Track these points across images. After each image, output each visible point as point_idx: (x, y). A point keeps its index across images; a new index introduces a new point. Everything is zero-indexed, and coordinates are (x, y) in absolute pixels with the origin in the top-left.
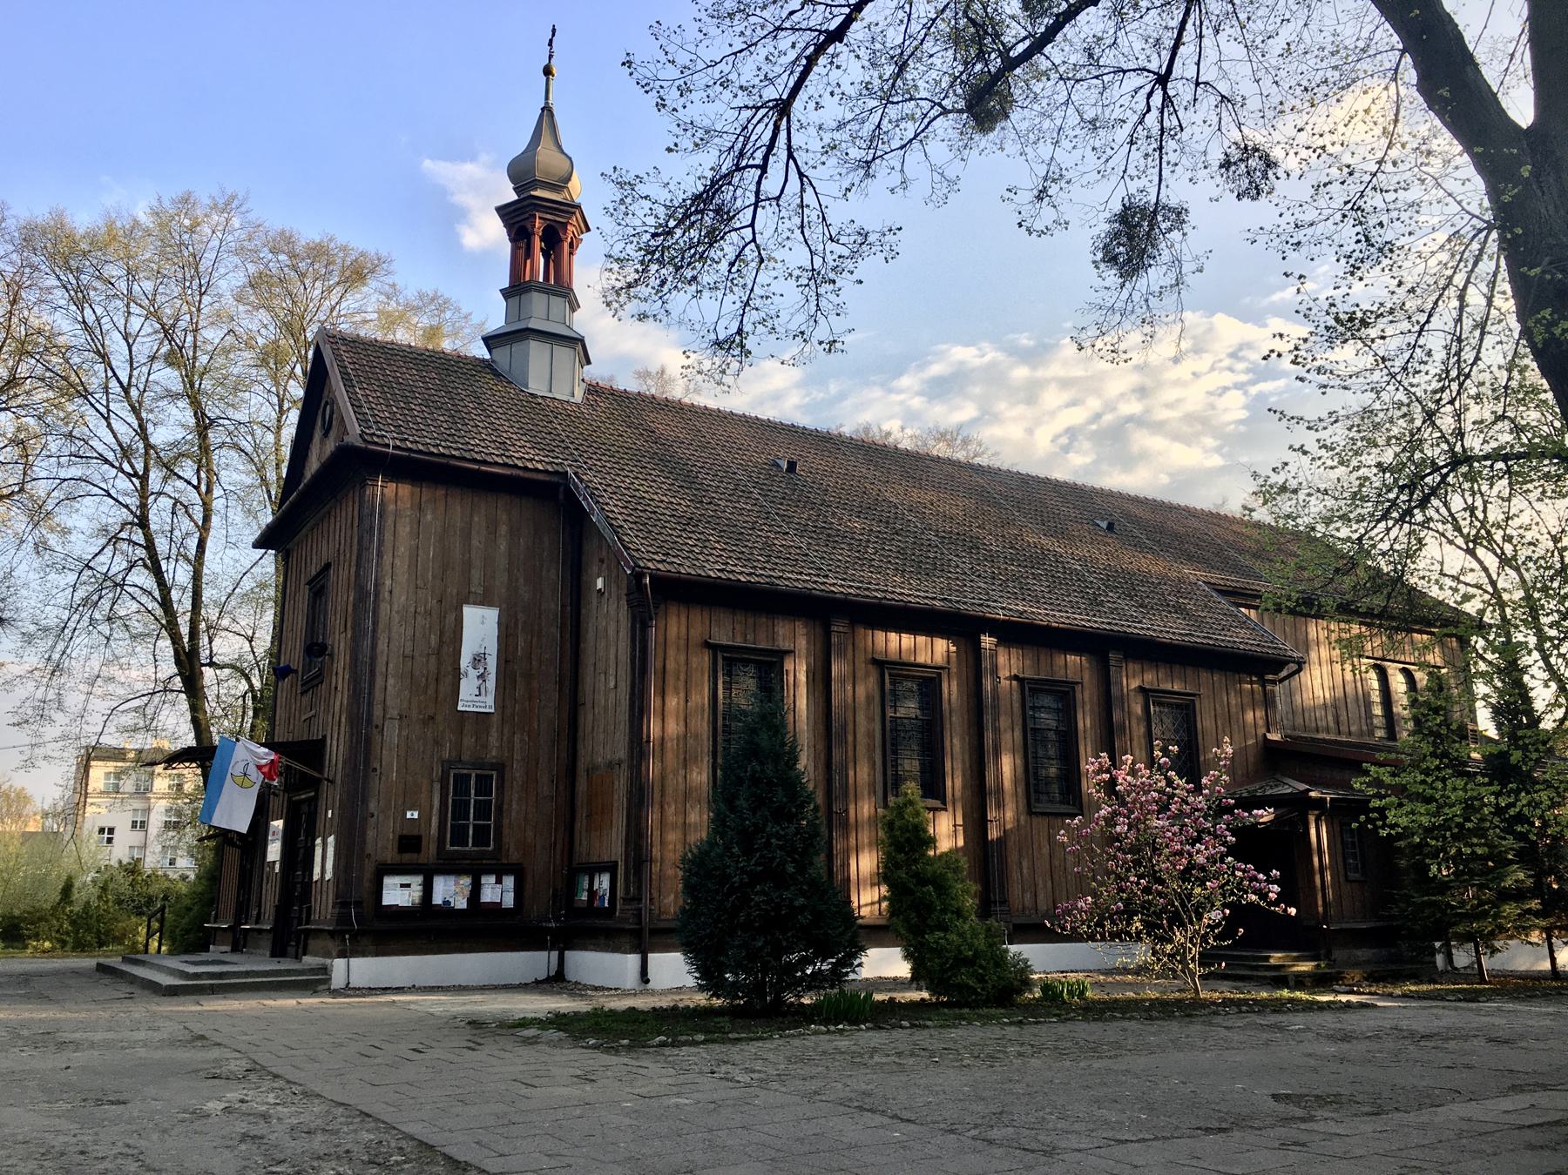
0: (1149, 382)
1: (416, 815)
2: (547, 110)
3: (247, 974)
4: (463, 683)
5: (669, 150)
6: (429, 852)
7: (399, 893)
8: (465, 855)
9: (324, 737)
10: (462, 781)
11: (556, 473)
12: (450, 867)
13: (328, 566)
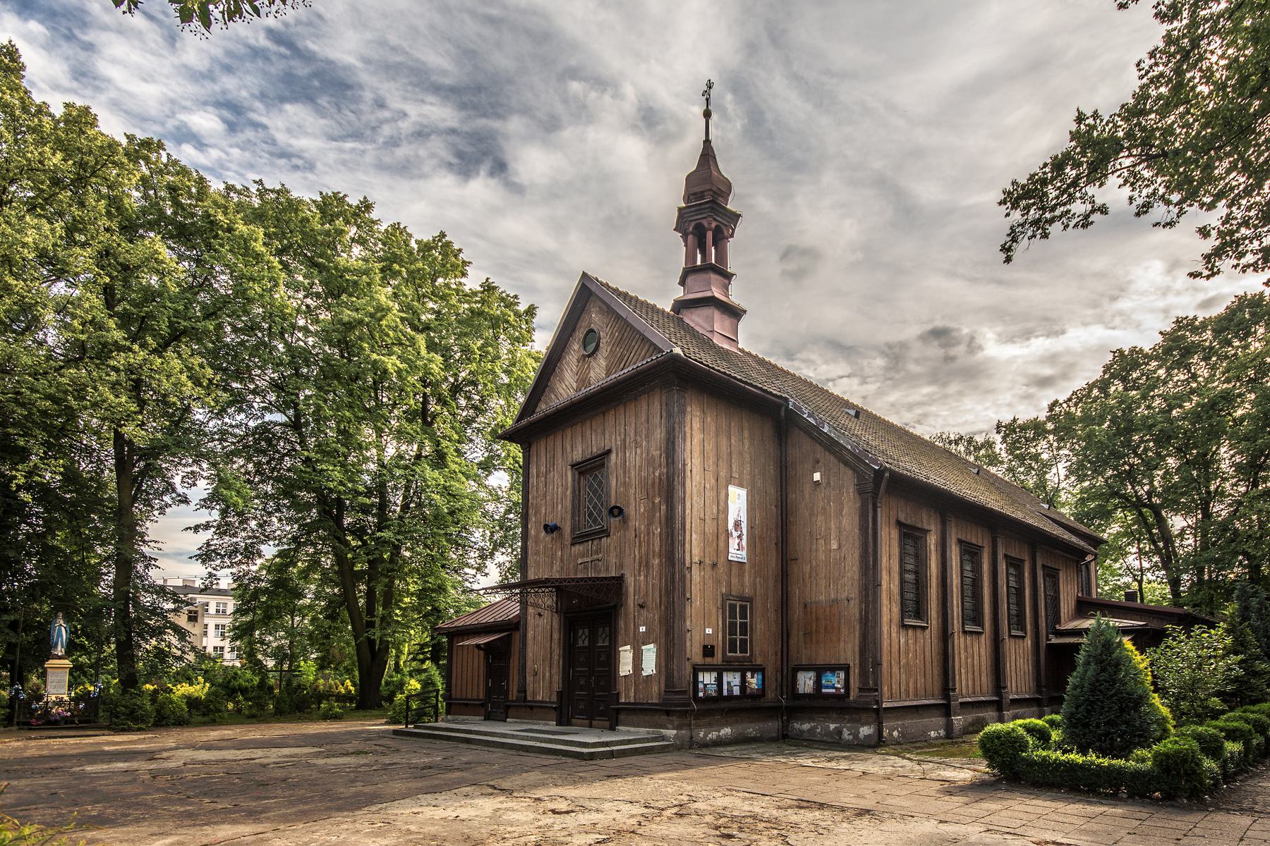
0: (217, 68)
2: (707, 142)
4: (731, 540)
5: (1008, 260)
8: (737, 659)
9: (623, 575)
10: (733, 607)
12: (728, 666)
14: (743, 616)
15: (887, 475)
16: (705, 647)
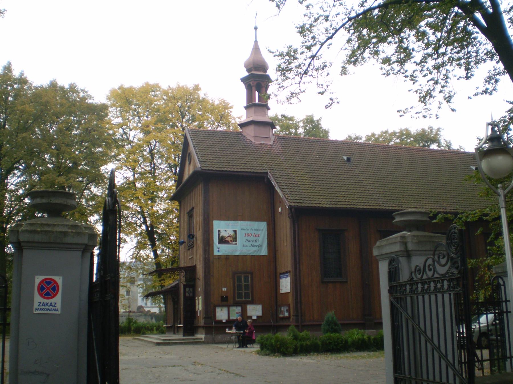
1: (225, 289)
2: (256, 42)
3: (173, 340)
6: (231, 300)
7: (222, 314)
11: (264, 173)
13: (193, 209)
14: (246, 280)
15: (293, 210)
16: (222, 297)
